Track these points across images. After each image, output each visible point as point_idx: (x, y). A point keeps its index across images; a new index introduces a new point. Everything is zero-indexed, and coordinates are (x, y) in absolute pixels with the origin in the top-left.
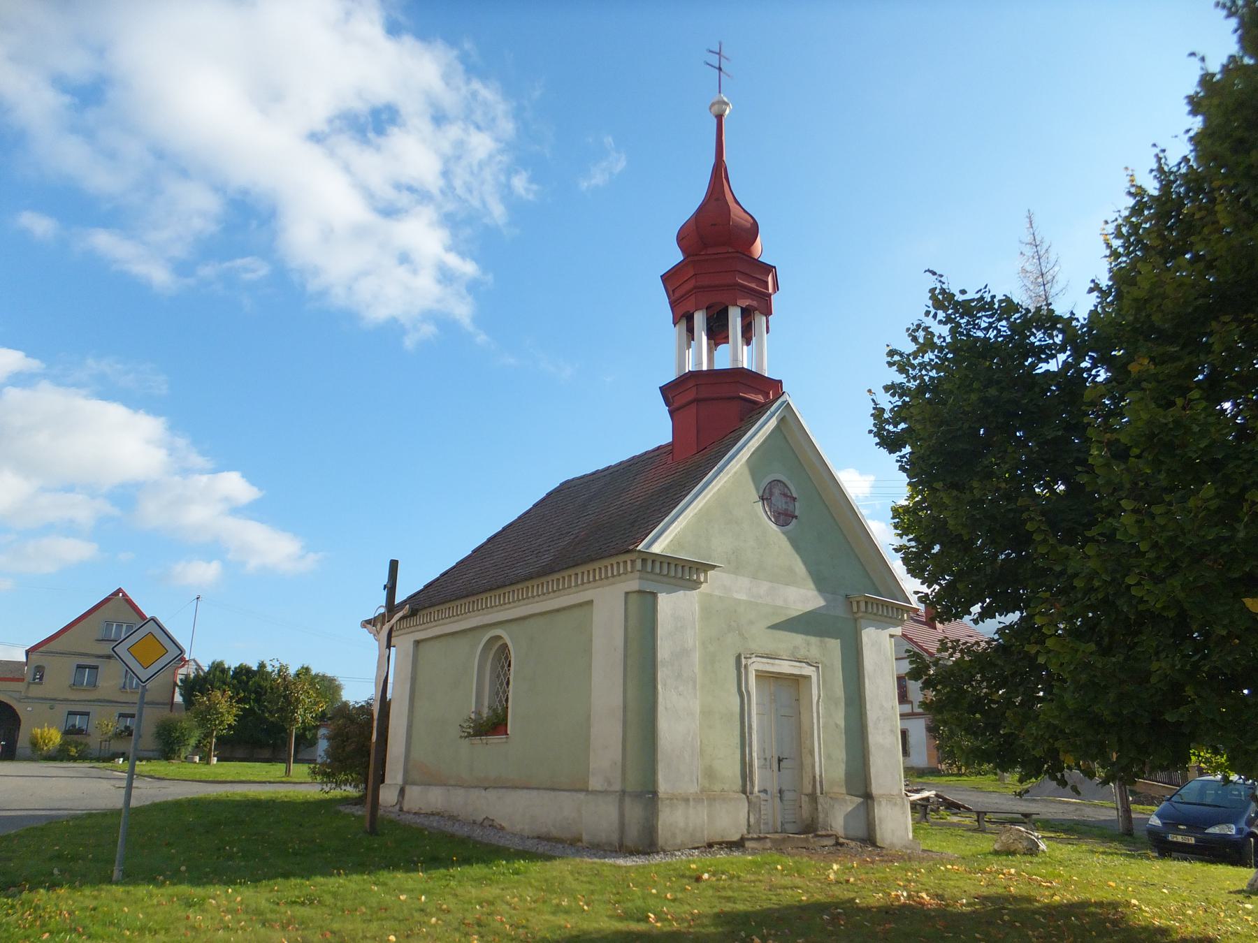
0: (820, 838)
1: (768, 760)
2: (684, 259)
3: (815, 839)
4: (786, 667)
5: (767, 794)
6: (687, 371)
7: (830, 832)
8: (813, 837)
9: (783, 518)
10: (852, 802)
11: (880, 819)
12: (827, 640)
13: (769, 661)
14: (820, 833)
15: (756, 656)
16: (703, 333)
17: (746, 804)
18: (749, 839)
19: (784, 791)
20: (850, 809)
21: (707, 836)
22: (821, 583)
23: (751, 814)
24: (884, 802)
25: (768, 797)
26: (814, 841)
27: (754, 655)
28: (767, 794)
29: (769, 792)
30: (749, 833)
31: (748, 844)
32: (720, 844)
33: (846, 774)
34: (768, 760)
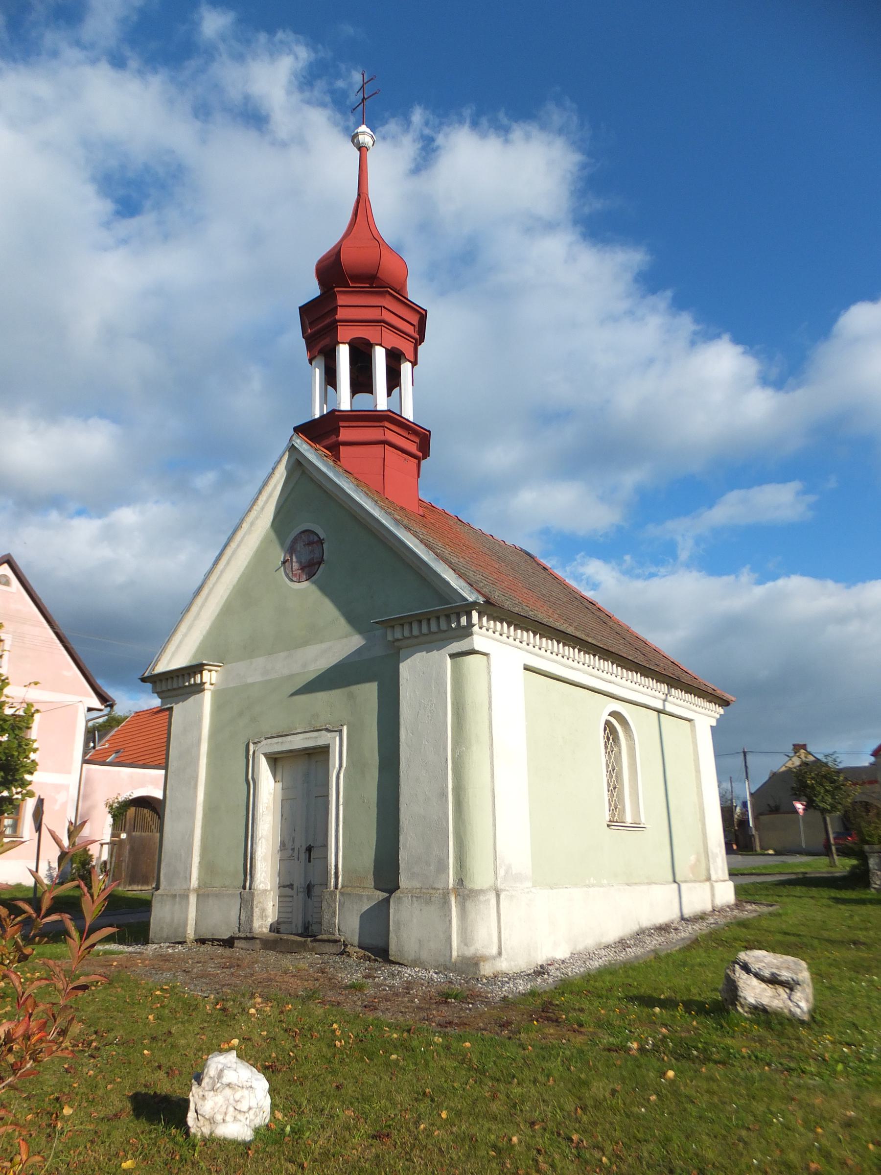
0: (321, 943)
1: (296, 851)
2: (321, 295)
3: (314, 944)
4: (298, 742)
5: (292, 889)
6: (317, 416)
7: (337, 937)
8: (311, 941)
9: (310, 569)
10: (369, 898)
11: (398, 923)
12: (355, 688)
13: (280, 739)
14: (319, 937)
15: (266, 739)
16: (317, 370)
17: (239, 900)
18: (239, 938)
19: (314, 886)
20: (366, 908)
21: (645, 990)
22: (355, 621)
23: (242, 911)
24: (406, 901)
25: (294, 893)
26: (314, 947)
27: (262, 739)
28: (292, 889)
29: (295, 887)
30: (239, 931)
31: (237, 943)
32: (213, 940)
33: (377, 861)
34: (296, 851)
